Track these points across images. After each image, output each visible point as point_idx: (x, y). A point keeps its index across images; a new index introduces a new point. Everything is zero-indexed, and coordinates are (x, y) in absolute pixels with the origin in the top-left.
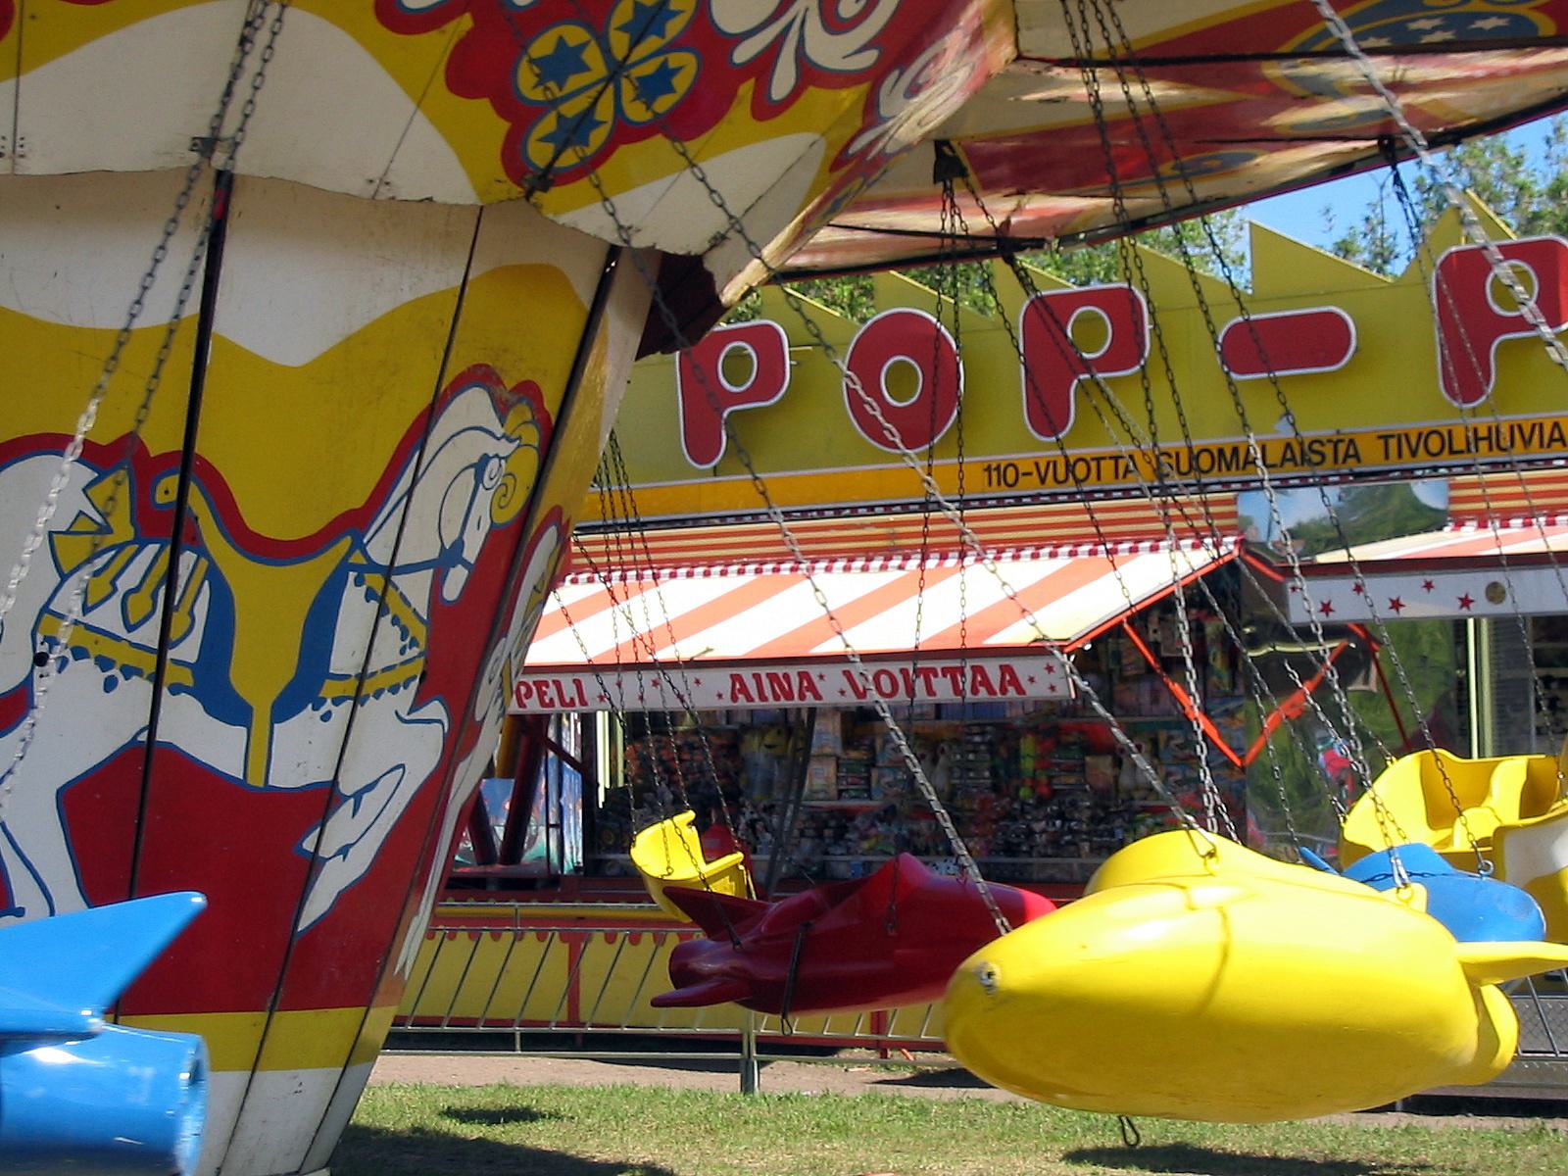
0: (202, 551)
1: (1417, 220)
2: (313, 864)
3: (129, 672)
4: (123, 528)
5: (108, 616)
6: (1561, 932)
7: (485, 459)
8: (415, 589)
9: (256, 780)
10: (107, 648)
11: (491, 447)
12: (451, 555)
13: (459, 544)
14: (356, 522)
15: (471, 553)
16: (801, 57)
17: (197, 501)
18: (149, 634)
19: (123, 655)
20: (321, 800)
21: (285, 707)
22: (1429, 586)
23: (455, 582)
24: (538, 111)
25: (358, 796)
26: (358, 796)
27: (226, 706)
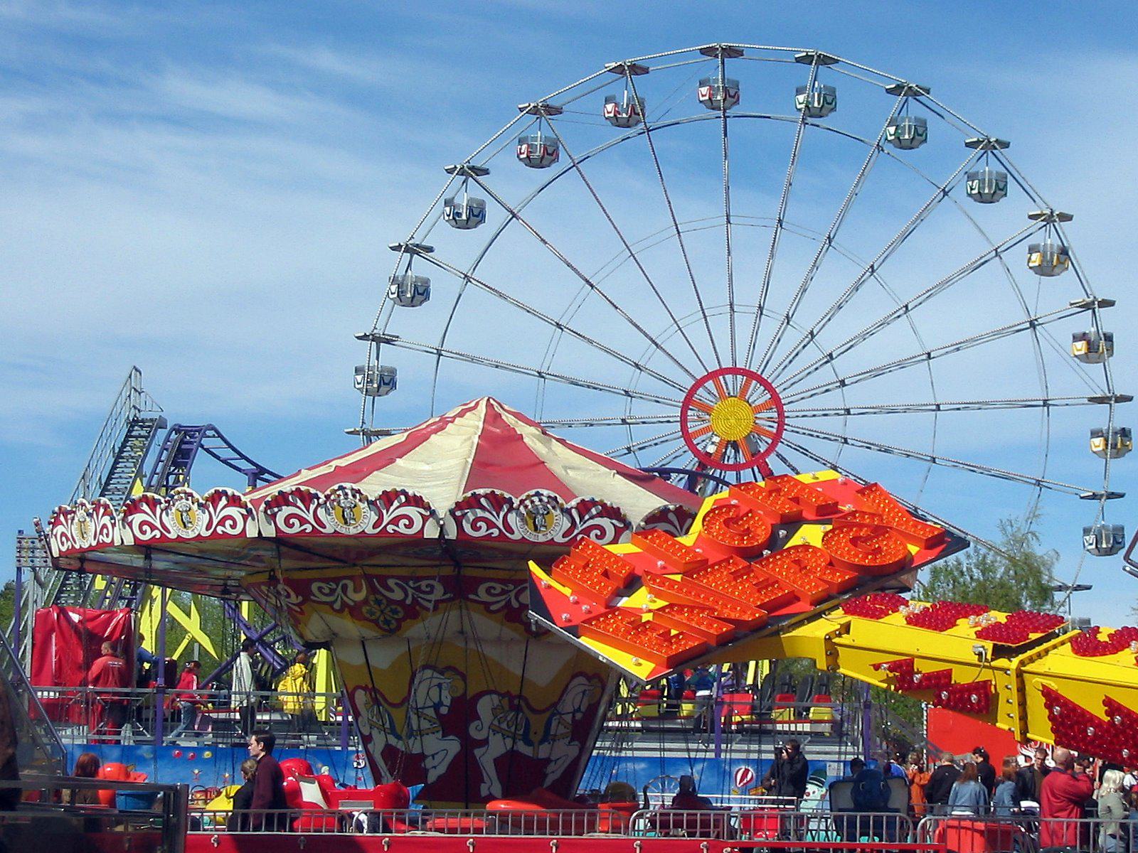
0: (524, 713)
1: (1067, 254)
2: (546, 776)
3: (508, 737)
4: (507, 708)
5: (504, 726)
6: (1133, 852)
7: (585, 690)
8: (568, 718)
9: (535, 758)
10: (504, 732)
11: (586, 688)
12: (579, 710)
13: (579, 708)
14: (555, 705)
15: (583, 709)
16: (62, 524)
17: (522, 703)
18: (513, 729)
19: (507, 733)
20: (548, 761)
21: (541, 742)
22: (918, 650)
23: (579, 716)
24: (396, 620)
25: (556, 761)
26: (556, 761)
27: (528, 742)
